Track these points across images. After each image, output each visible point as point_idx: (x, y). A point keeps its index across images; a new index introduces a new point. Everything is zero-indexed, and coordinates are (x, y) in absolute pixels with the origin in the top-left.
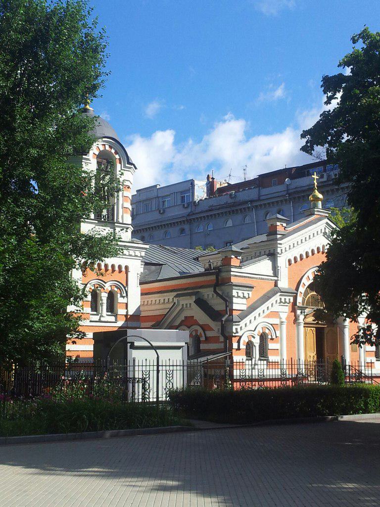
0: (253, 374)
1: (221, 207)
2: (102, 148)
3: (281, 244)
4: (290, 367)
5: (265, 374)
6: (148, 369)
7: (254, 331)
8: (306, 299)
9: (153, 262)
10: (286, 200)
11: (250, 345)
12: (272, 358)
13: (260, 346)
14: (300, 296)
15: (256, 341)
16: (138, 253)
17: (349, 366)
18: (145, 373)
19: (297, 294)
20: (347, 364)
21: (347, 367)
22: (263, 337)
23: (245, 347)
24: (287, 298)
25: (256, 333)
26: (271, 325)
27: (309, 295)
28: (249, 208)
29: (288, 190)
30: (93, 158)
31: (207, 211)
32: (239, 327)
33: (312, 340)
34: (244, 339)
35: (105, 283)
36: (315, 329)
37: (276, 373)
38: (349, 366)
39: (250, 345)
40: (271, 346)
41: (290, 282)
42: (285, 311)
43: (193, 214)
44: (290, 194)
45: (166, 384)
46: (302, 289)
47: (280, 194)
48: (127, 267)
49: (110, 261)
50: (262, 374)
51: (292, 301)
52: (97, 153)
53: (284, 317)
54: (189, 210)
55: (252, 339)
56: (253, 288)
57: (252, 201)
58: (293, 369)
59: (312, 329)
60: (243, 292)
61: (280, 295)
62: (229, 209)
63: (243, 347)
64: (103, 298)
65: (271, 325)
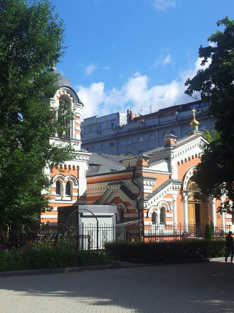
0: (157, 232)
1: (136, 129)
2: (62, 93)
3: (173, 152)
4: (181, 227)
5: (164, 232)
6: (91, 230)
7: (157, 206)
8: (189, 186)
9: (94, 163)
10: (176, 125)
11: (154, 215)
12: (168, 223)
13: (160, 215)
14: (185, 184)
15: (158, 212)
16: (85, 158)
17: (216, 227)
18: (90, 232)
19: (183, 183)
20: (215, 226)
21: (215, 228)
22: (162, 210)
23: (151, 216)
24: (177, 186)
25: (158, 207)
26: (167, 202)
27: (191, 184)
28: (153, 130)
29: (177, 119)
30: (57, 99)
31: (127, 132)
32: (147, 204)
33: (193, 212)
34: (151, 211)
35: (65, 176)
36: (194, 204)
37: (171, 232)
38: (216, 227)
39: (154, 215)
40: (168, 215)
41: (179, 177)
42: (176, 194)
43: (119, 134)
44: (178, 122)
45: (103, 239)
46: (186, 180)
47: (172, 121)
48: (78, 167)
49: (67, 163)
50: (162, 232)
51: (180, 187)
52: (59, 96)
53: (175, 197)
54: (116, 131)
55: (156, 211)
56: (156, 179)
57: (155, 126)
58: (181, 230)
59: (193, 204)
60: (150, 182)
61: (173, 184)
62: (141, 131)
63: (150, 216)
64: (63, 186)
65: (167, 202)
